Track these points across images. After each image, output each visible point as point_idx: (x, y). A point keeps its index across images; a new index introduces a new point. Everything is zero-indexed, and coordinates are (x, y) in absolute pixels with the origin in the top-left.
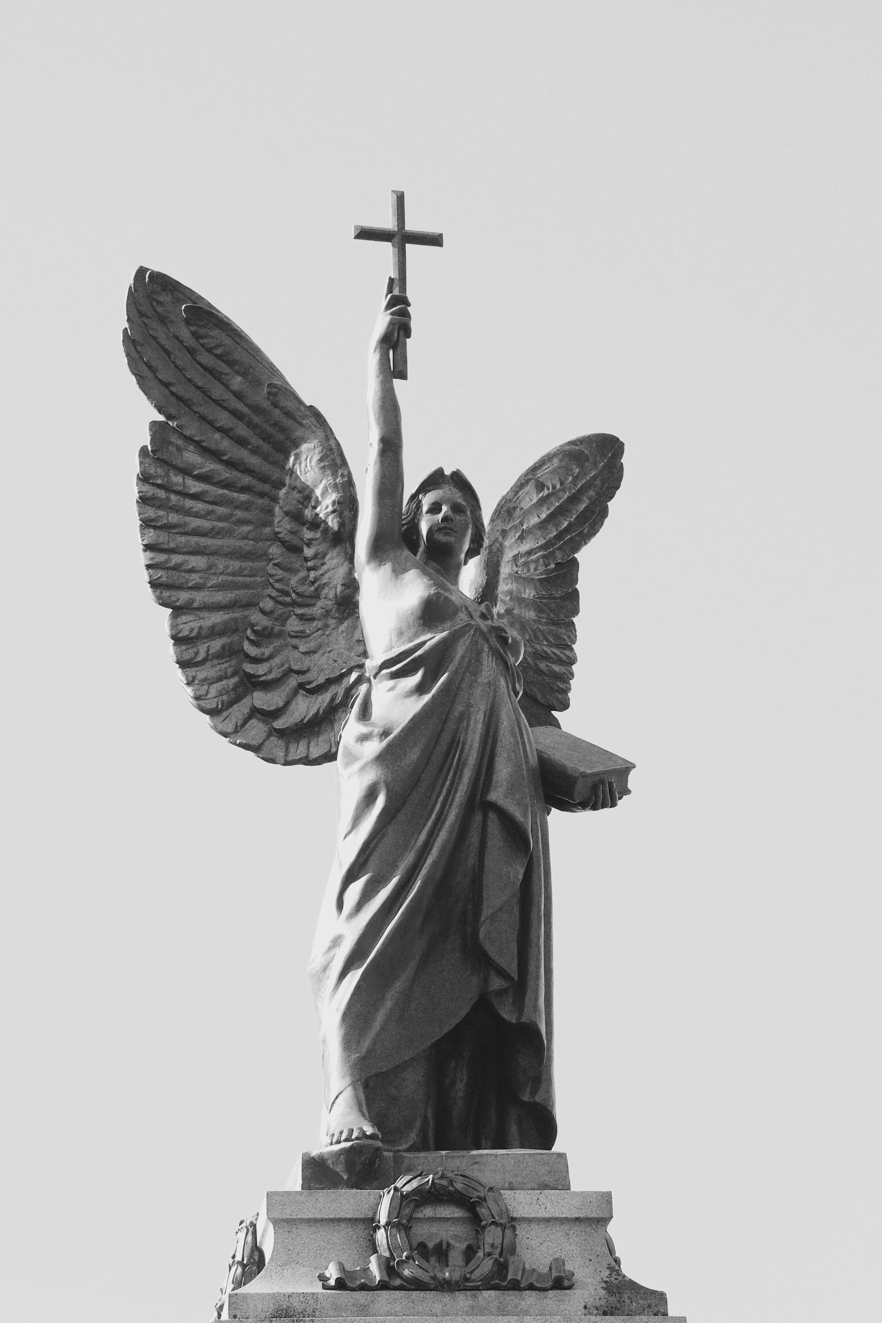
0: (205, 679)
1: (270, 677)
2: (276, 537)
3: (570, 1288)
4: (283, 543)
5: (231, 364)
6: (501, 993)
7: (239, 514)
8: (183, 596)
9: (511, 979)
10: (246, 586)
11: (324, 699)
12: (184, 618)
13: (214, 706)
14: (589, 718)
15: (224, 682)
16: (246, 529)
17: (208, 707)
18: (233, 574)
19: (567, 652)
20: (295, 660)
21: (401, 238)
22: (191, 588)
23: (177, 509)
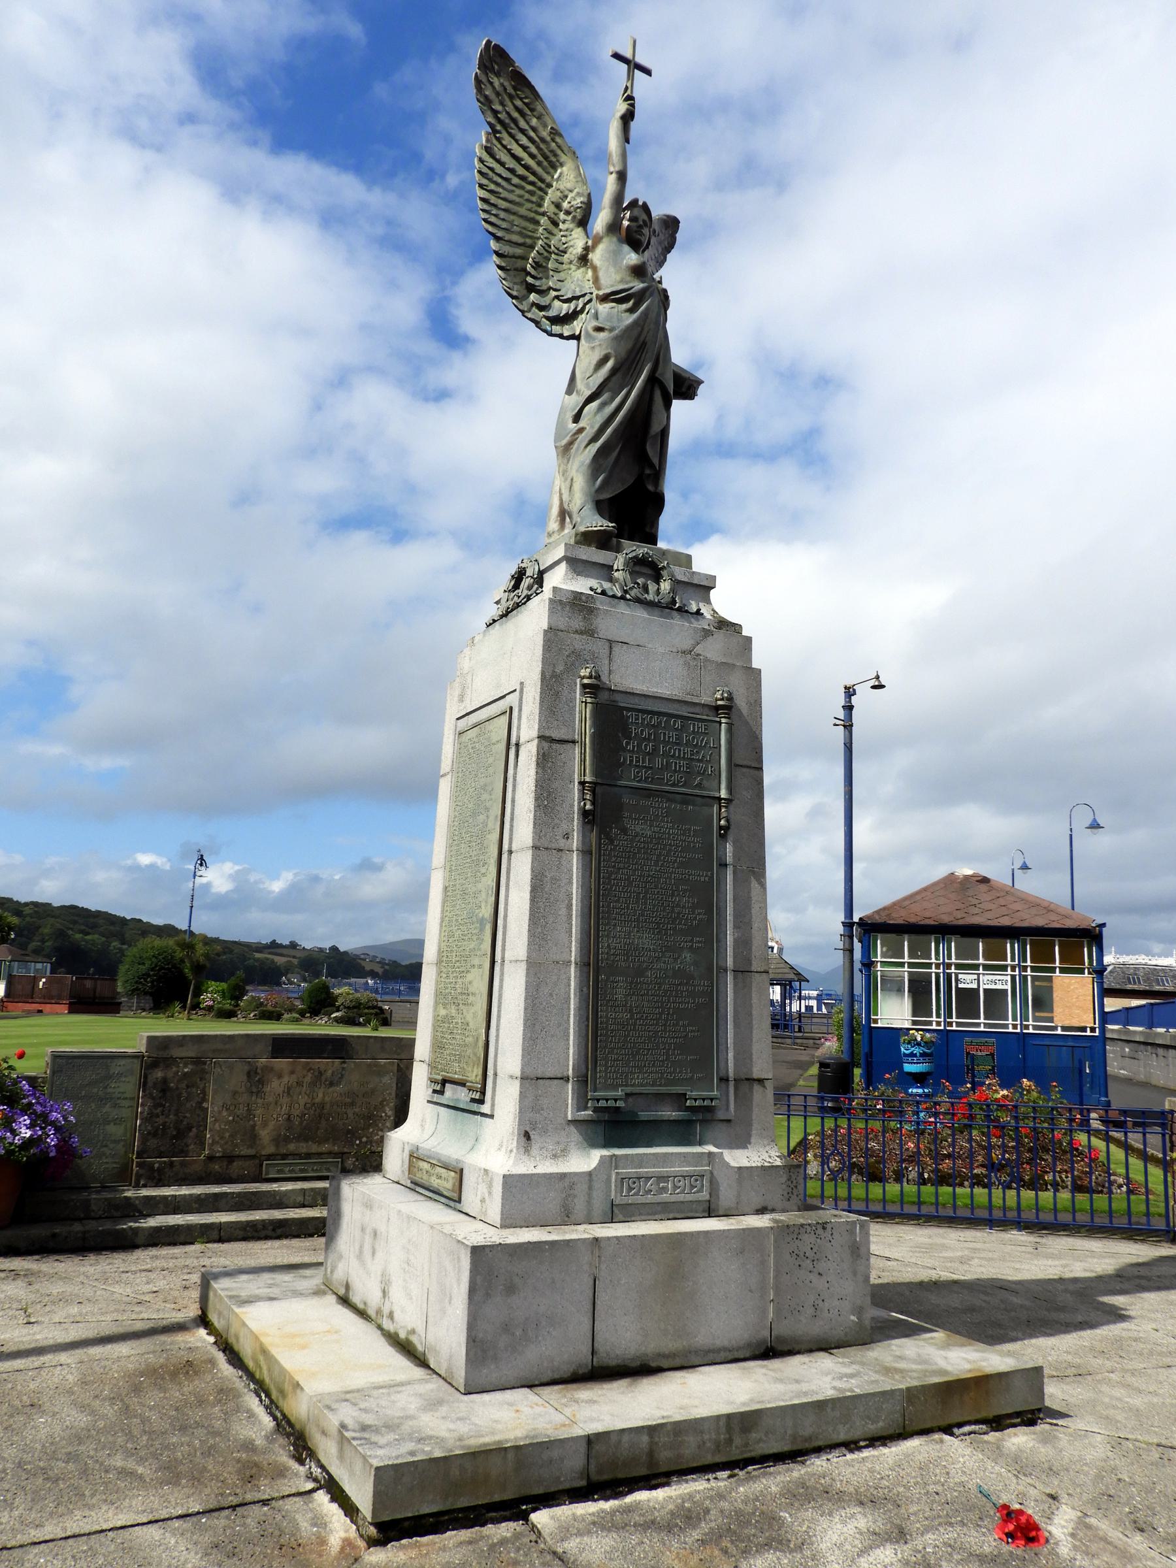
5: (532, 110)
6: (649, 475)
11: (572, 305)
21: (634, 66)
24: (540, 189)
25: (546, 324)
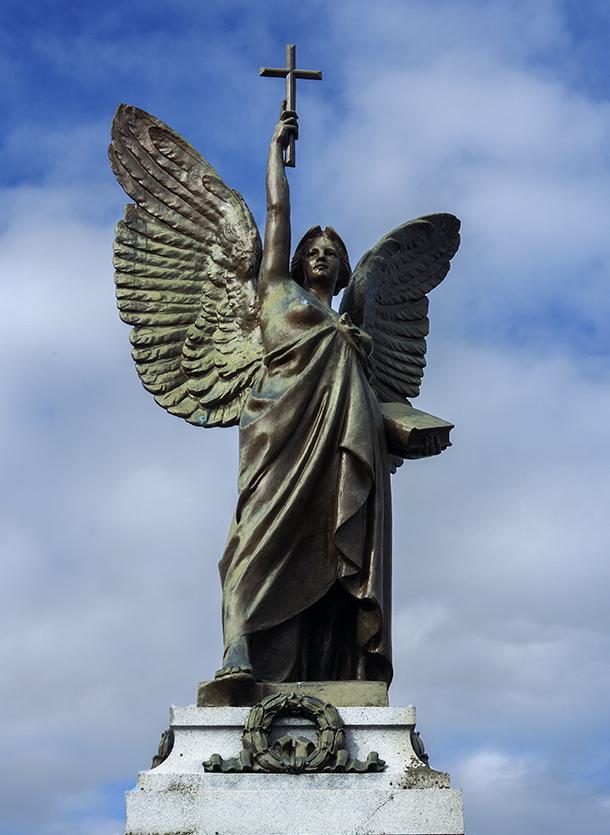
0: (155, 372)
1: (200, 370)
2: (208, 278)
3: (382, 771)
4: (213, 281)
5: (180, 164)
7: (183, 263)
8: (142, 317)
9: (358, 567)
10: (188, 310)
11: (235, 382)
12: (142, 332)
13: (158, 389)
14: (429, 404)
15: (170, 373)
16: (187, 273)
17: (155, 389)
18: (178, 303)
19: (420, 359)
20: (215, 357)
22: (149, 312)
23: (142, 261)
24: (199, 250)
25: (201, 415)
